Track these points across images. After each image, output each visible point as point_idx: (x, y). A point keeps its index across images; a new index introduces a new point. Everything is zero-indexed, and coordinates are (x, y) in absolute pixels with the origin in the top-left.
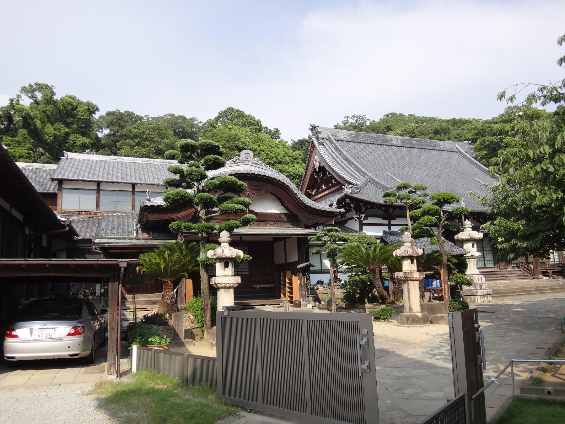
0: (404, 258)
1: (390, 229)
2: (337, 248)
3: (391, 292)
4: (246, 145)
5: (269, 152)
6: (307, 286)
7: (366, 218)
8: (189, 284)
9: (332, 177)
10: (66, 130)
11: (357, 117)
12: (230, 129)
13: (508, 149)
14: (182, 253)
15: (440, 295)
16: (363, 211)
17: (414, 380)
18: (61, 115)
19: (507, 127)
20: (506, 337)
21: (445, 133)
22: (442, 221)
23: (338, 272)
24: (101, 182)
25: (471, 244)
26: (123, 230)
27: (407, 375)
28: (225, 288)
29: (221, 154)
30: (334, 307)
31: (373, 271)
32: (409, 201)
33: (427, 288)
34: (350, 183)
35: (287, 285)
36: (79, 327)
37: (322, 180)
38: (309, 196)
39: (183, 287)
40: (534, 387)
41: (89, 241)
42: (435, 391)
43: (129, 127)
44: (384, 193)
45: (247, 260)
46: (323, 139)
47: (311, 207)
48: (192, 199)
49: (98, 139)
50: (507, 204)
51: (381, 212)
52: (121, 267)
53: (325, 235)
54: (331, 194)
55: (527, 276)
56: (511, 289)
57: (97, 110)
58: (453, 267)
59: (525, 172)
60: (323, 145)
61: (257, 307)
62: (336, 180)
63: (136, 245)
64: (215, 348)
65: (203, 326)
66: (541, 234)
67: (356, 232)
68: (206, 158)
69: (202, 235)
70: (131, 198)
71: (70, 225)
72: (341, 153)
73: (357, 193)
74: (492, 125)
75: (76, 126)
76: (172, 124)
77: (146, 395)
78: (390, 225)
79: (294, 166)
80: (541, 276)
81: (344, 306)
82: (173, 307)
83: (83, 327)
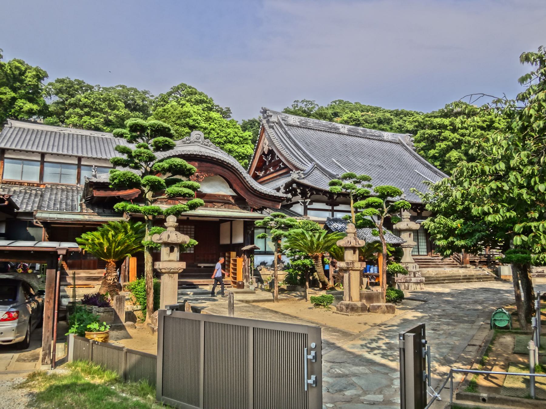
0: (346, 248)
1: (333, 216)
2: (282, 234)
3: (331, 276)
4: (197, 123)
5: (219, 132)
6: (251, 268)
7: (311, 203)
8: (132, 262)
9: (280, 161)
10: (13, 94)
11: (306, 102)
12: (183, 105)
13: (445, 142)
14: (126, 233)
15: (377, 281)
16: (308, 195)
17: (354, 379)
18: (8, 79)
19: (446, 121)
20: (439, 331)
21: (388, 123)
22: (384, 214)
24: (46, 153)
25: (408, 233)
26: (66, 205)
27: (347, 372)
28: (169, 273)
29: (171, 136)
30: (276, 290)
31: (316, 258)
32: (354, 191)
33: (365, 273)
34: (297, 169)
35: (231, 266)
36: (13, 312)
37: (269, 163)
38: (256, 177)
39: (127, 265)
40: (470, 393)
41: (30, 214)
42: (375, 393)
43: (78, 96)
44: (331, 181)
45: (193, 245)
46: (273, 123)
47: (258, 191)
48: (139, 181)
49: (46, 107)
50: (447, 203)
51: (325, 198)
52: (60, 255)
53: (272, 220)
54: (278, 177)
55: (457, 264)
56: (441, 277)
57: (47, 76)
58: (390, 255)
59: (480, 188)
60: (273, 129)
61: (200, 287)
62: (284, 164)
63: (79, 221)
64: (156, 333)
65: (145, 308)
66: (478, 234)
67: (301, 216)
68: (156, 139)
69: (148, 217)
70: (77, 171)
71: (9, 199)
72: (290, 138)
73: (303, 178)
74: (432, 119)
75: (23, 91)
76: (123, 95)
77: (81, 392)
78: (333, 211)
79: (243, 147)
80: (468, 265)
81: (285, 288)
82: (116, 288)
83: (17, 312)
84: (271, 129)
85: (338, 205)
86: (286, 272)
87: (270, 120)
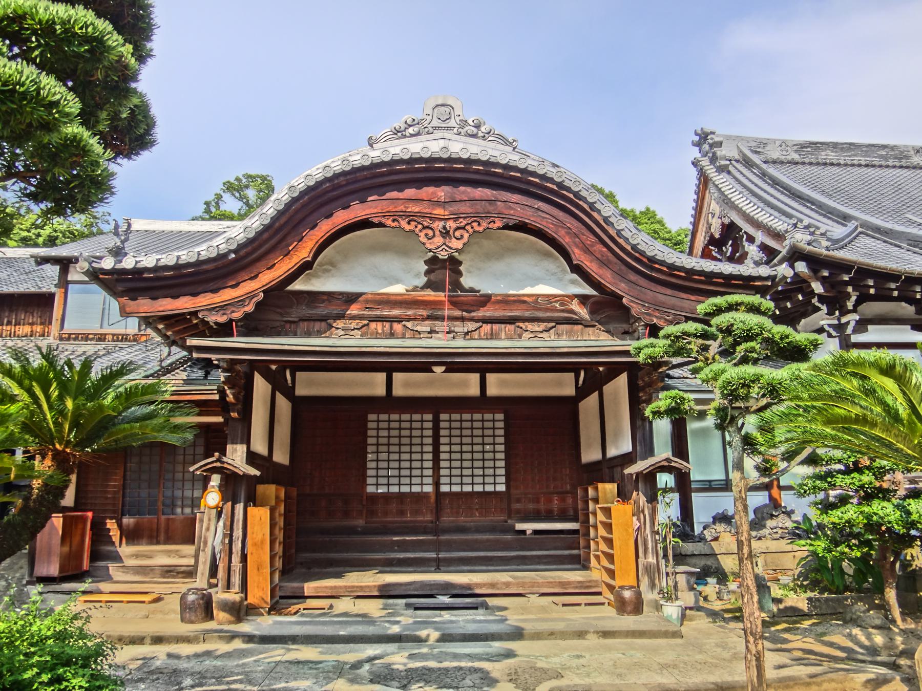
7: (862, 325)
16: (850, 305)
23: (781, 488)
60: (729, 172)
84: (724, 174)
86: (803, 548)
87: (719, 153)
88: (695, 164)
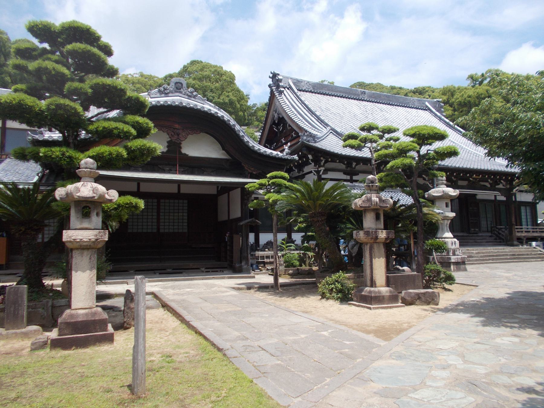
7: (326, 171)
9: (292, 130)
51: (342, 166)
72: (302, 103)
85: (357, 174)
88: (270, 86)
